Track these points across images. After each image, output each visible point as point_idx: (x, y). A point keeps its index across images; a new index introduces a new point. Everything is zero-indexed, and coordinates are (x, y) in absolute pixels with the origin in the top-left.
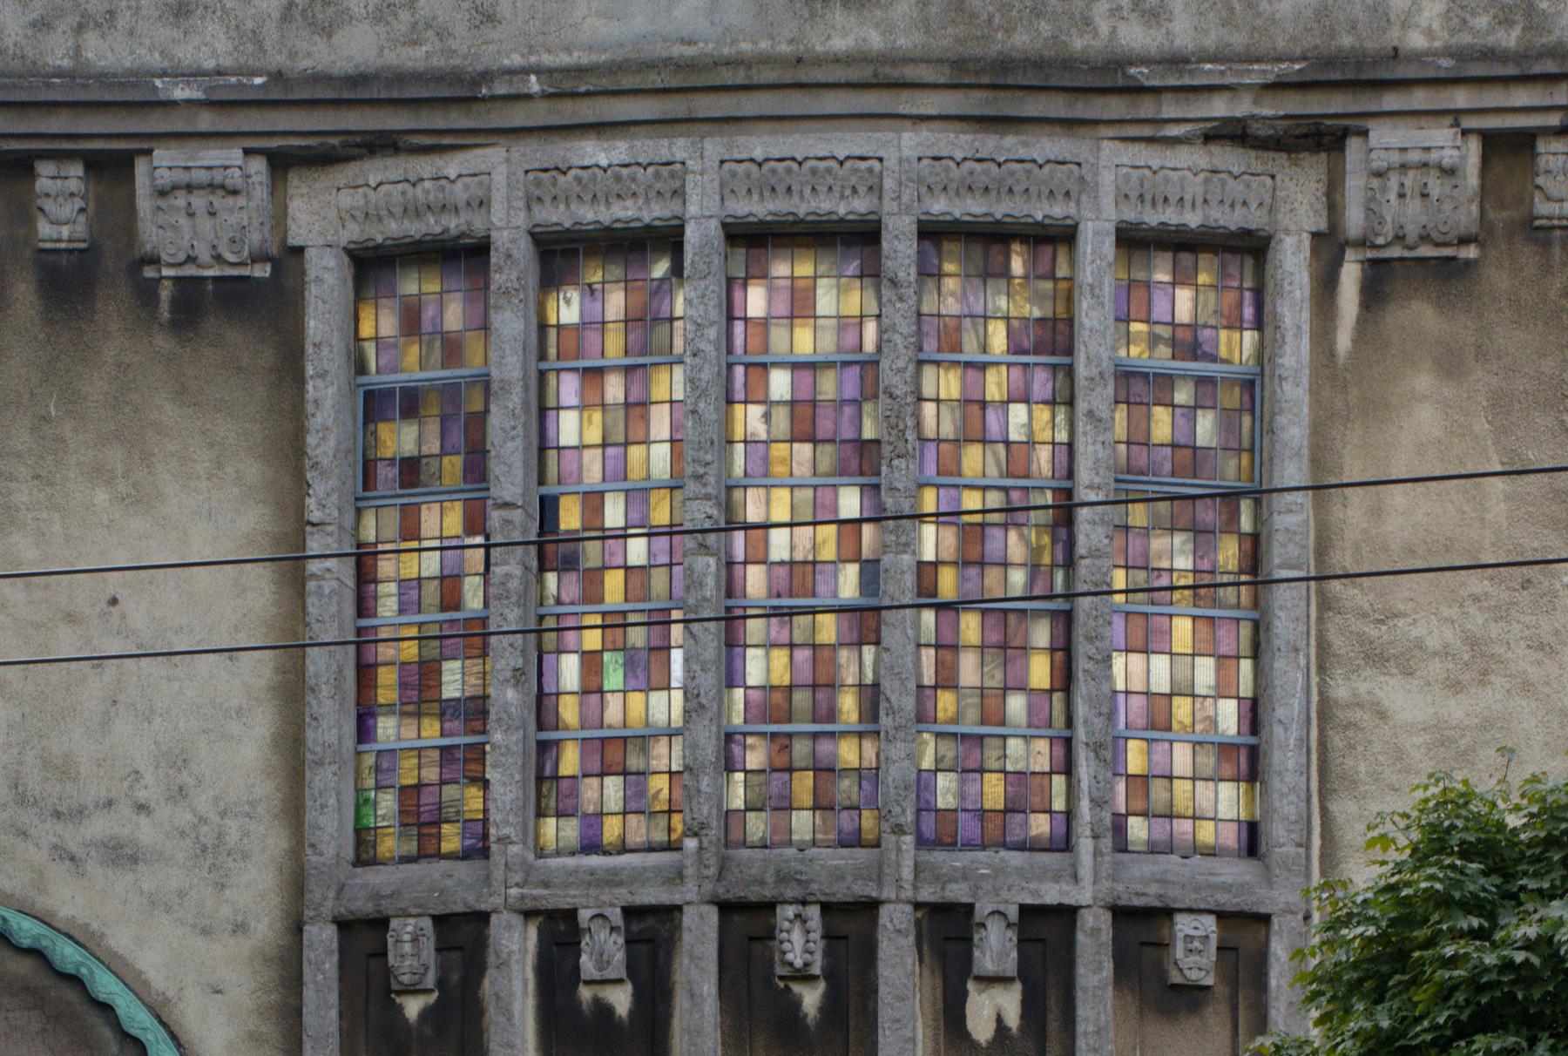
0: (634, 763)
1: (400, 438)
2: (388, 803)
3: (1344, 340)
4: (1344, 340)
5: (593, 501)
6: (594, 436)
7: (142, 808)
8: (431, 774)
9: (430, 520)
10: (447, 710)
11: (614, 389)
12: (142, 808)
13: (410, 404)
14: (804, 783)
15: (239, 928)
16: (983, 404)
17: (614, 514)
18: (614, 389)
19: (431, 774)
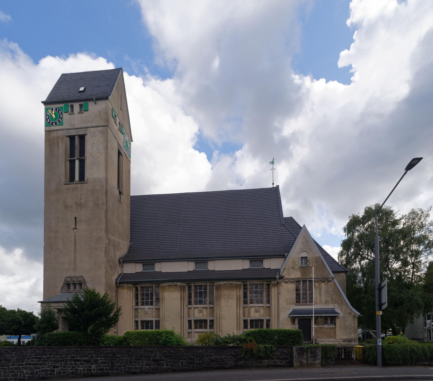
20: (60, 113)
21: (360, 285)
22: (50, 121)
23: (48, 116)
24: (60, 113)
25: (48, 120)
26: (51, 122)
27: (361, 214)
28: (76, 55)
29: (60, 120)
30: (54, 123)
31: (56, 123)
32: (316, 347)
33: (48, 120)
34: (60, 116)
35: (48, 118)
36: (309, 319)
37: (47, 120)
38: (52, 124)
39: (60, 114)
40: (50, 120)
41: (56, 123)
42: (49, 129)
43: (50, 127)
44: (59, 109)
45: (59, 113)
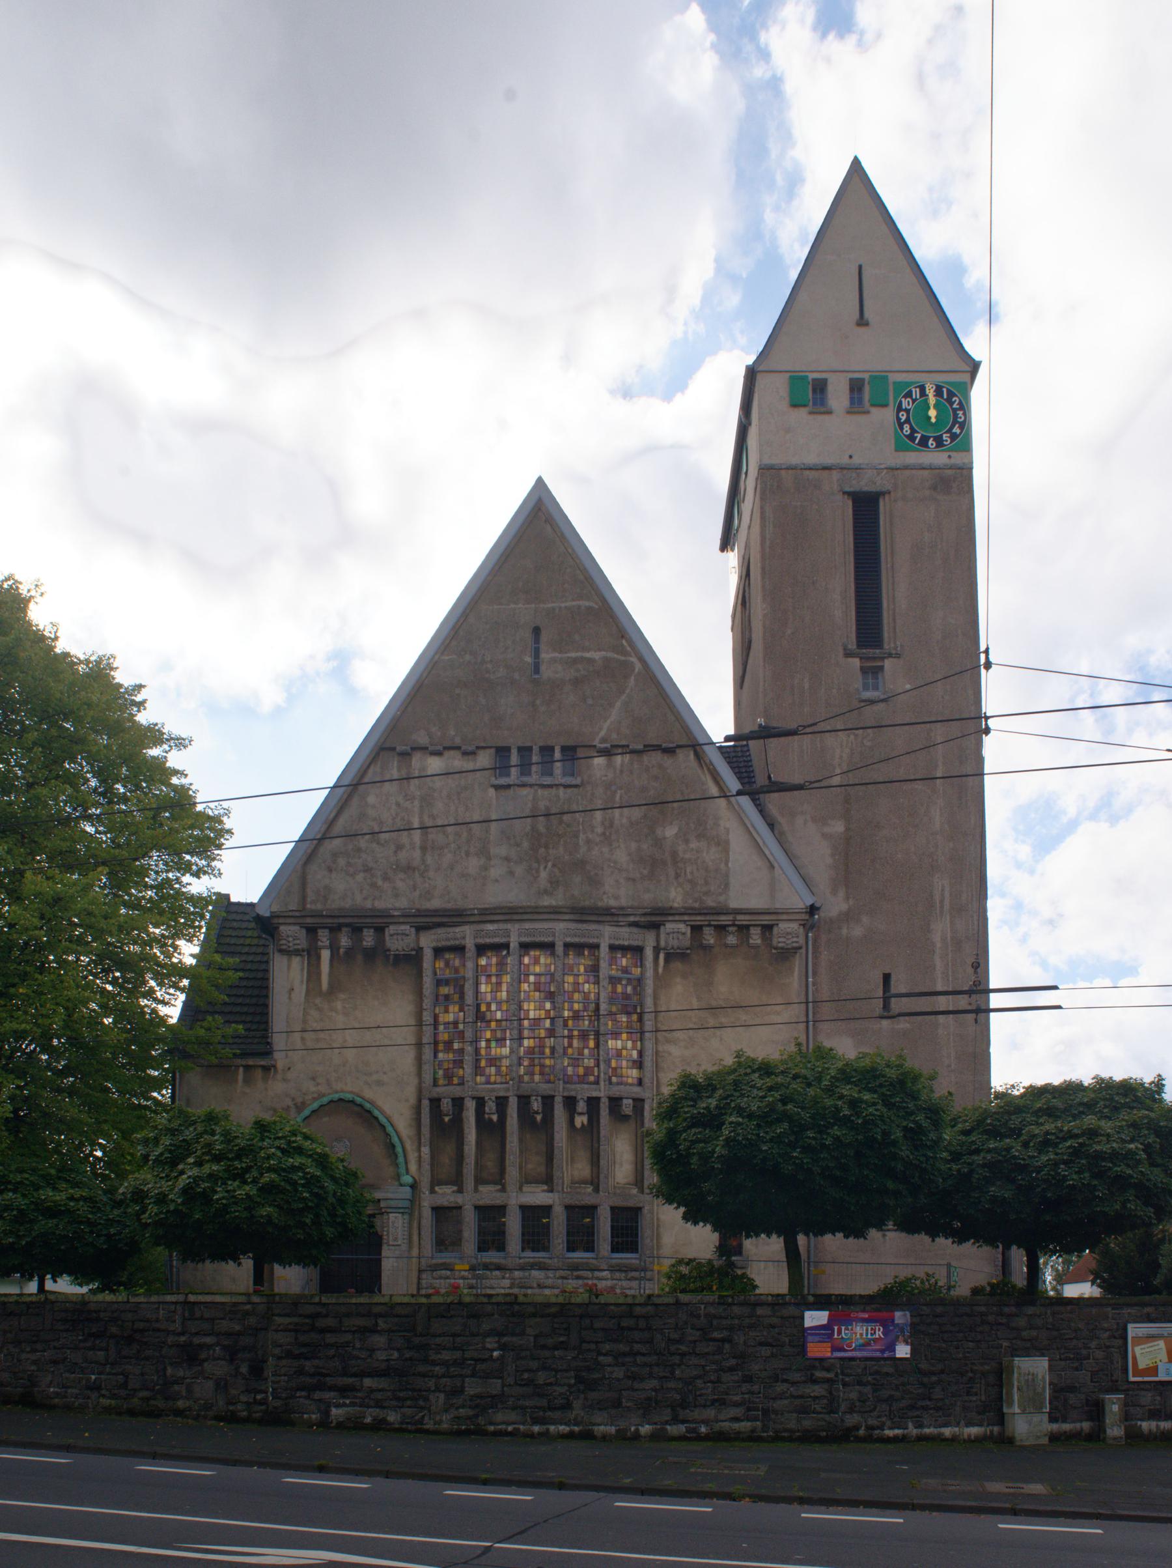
0: (498, 1064)
1: (445, 990)
2: (441, 1072)
3: (660, 970)
4: (660, 970)
5: (489, 1005)
6: (489, 990)
7: (385, 1073)
8: (451, 1066)
9: (451, 1008)
10: (454, 1051)
11: (494, 979)
12: (385, 1073)
13: (447, 982)
14: (537, 1069)
15: (407, 1100)
16: (578, 984)
17: (493, 1007)
18: (494, 979)
19: (451, 1066)
20: (955, 406)
21: (497, 1021)
22: (913, 431)
23: (907, 411)
24: (955, 406)
25: (907, 428)
26: (919, 436)
27: (554, 789)
28: (824, 36)
29: (956, 430)
30: (931, 441)
31: (939, 442)
32: (788, 933)
33: (907, 428)
34: (955, 416)
35: (908, 421)
36: (655, 991)
37: (960, 403)
38: (924, 442)
39: (954, 410)
40: (912, 428)
41: (939, 442)
42: (947, 461)
43: (951, 453)
44: (948, 390)
45: (951, 404)
